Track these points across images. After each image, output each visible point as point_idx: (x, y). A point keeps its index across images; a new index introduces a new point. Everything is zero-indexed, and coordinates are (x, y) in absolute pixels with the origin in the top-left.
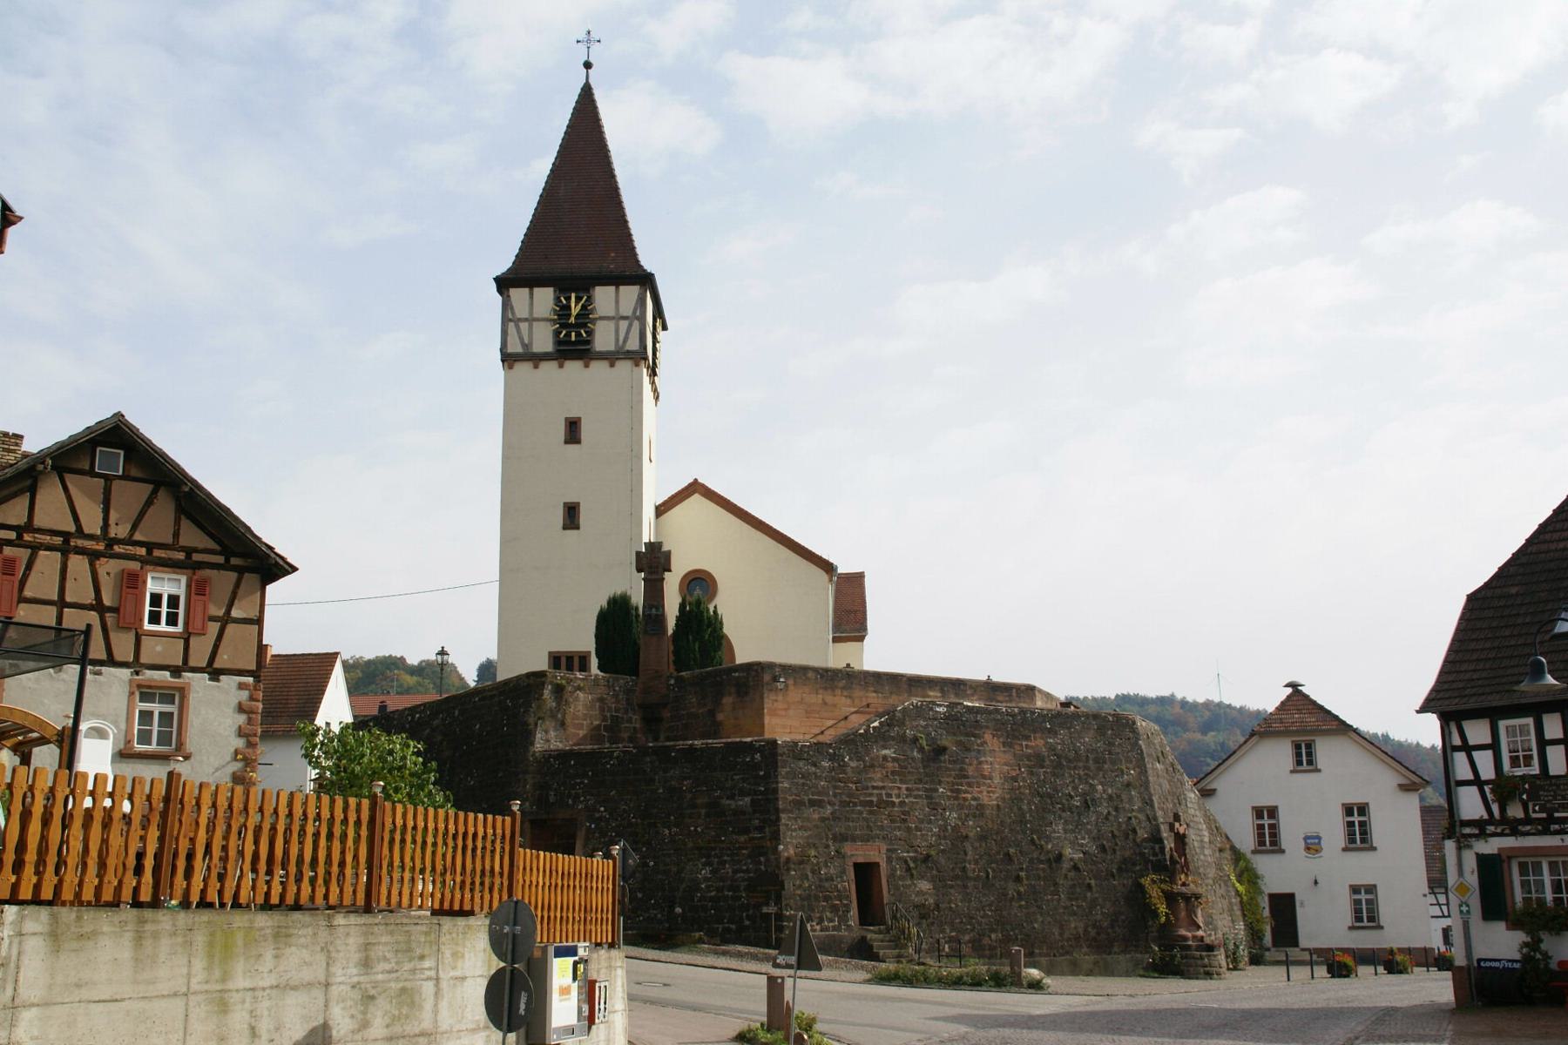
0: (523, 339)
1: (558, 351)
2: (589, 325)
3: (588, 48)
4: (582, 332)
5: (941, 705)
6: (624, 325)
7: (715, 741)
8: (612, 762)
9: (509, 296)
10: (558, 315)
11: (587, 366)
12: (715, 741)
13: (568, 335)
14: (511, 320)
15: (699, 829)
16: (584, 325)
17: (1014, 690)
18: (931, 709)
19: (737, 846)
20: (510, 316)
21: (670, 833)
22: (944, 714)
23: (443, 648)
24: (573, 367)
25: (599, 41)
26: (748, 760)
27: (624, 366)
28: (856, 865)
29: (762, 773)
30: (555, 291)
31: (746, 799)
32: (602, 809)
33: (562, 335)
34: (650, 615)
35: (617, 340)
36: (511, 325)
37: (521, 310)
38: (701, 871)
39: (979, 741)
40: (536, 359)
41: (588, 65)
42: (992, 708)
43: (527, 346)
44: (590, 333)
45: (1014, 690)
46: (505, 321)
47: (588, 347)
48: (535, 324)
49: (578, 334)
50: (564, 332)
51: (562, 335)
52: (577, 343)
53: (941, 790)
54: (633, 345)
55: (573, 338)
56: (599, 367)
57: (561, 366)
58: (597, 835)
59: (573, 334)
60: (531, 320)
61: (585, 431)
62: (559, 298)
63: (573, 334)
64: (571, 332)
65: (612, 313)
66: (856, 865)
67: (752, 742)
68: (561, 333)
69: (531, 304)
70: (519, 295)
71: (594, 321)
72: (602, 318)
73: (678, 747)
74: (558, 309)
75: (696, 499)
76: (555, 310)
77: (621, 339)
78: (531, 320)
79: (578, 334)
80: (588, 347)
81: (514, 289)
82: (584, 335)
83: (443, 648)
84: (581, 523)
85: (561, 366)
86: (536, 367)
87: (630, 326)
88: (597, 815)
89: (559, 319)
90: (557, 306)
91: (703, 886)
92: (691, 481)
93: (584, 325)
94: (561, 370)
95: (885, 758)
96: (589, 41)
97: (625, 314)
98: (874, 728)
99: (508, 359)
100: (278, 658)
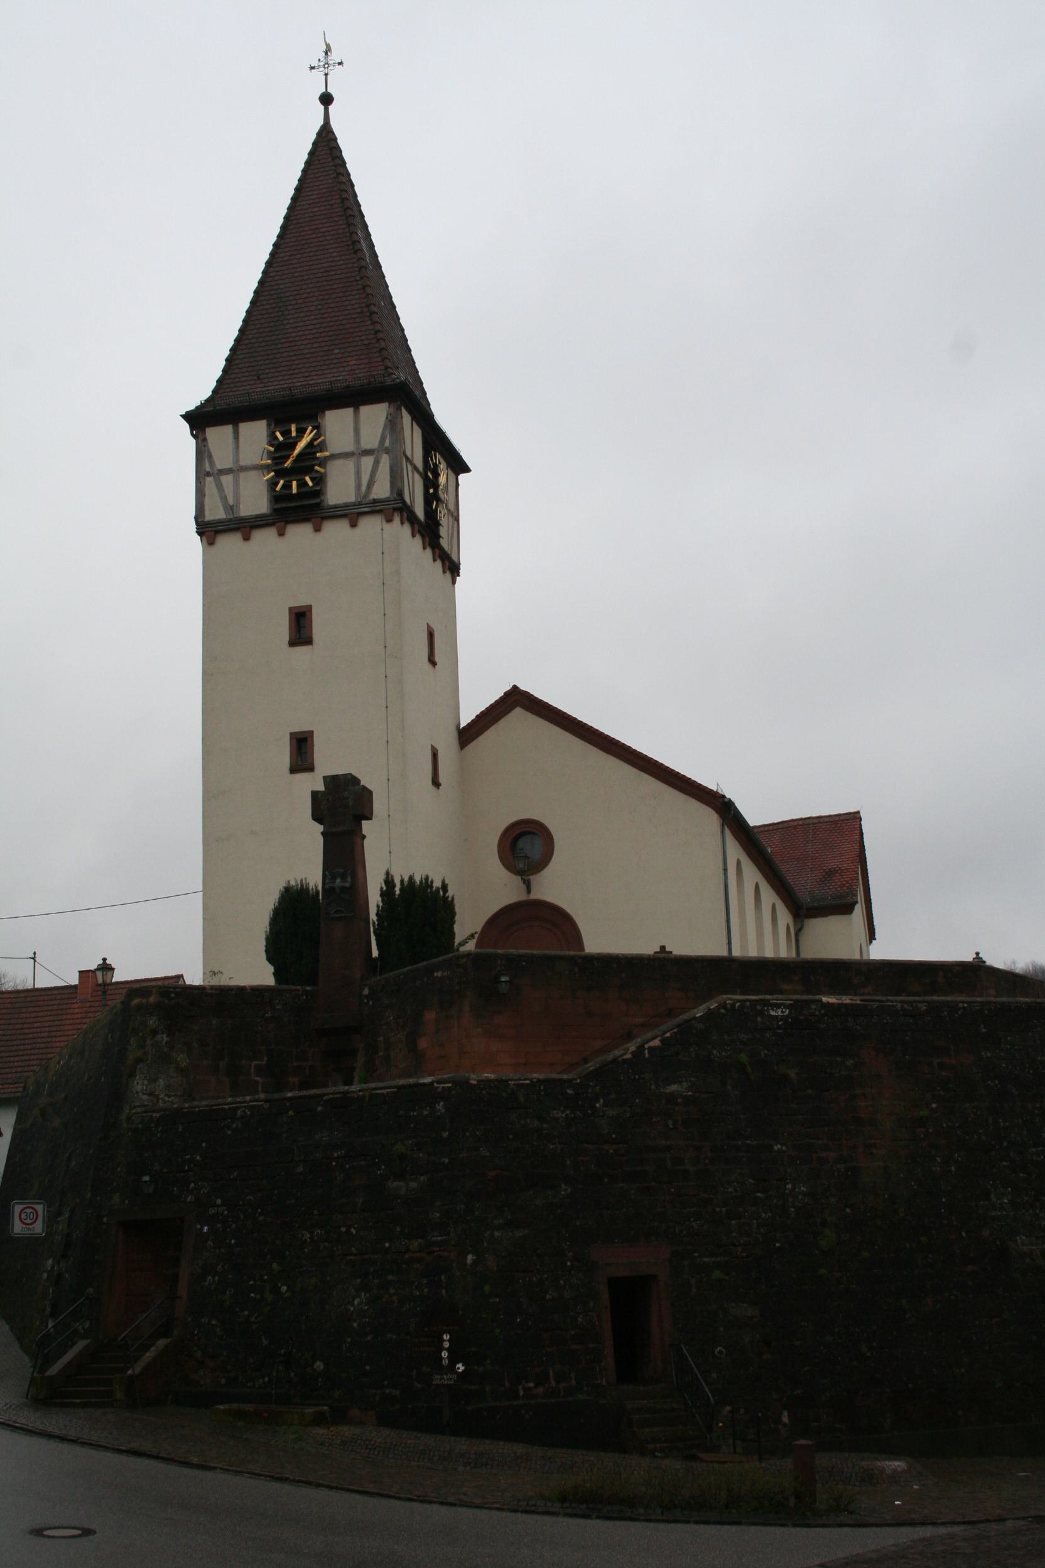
0: (226, 498)
1: (275, 510)
2: (317, 468)
3: (326, 75)
4: (307, 479)
5: (778, 1006)
6: (367, 462)
7: (381, 1085)
8: (234, 1126)
9: (205, 440)
10: (273, 459)
11: (317, 529)
12: (381, 1085)
13: (287, 486)
14: (208, 474)
15: (353, 1231)
16: (309, 470)
17: (941, 974)
18: (761, 1013)
19: (407, 1256)
20: (208, 468)
21: (311, 1238)
22: (784, 1018)
23: (977, 954)
24: (300, 533)
25: (340, 64)
26: (425, 1113)
27: (371, 525)
28: (613, 1283)
29: (445, 1135)
30: (269, 425)
31: (422, 1178)
32: (219, 1201)
33: (278, 488)
34: (333, 889)
35: (358, 486)
36: (209, 479)
37: (222, 457)
38: (354, 1299)
39: (850, 1062)
40: (245, 527)
41: (326, 99)
42: (875, 1005)
43: (232, 507)
44: (320, 480)
45: (941, 974)
46: (201, 475)
47: (318, 501)
48: (242, 475)
49: (302, 484)
50: (282, 482)
51: (278, 488)
52: (299, 496)
53: (777, 1147)
54: (382, 490)
55: (295, 491)
56: (336, 529)
57: (281, 534)
58: (210, 1243)
59: (294, 484)
60: (236, 470)
61: (319, 626)
62: (274, 433)
63: (294, 484)
64: (291, 482)
65: (350, 447)
66: (613, 1283)
67: (432, 1084)
68: (276, 484)
69: (237, 447)
70: (219, 436)
71: (323, 463)
72: (333, 457)
73: (326, 1098)
74: (272, 449)
75: (518, 713)
76: (269, 452)
77: (364, 488)
78: (236, 470)
79: (302, 484)
80: (318, 501)
81: (211, 428)
82: (310, 484)
83: (977, 954)
84: (316, 762)
85: (281, 534)
86: (247, 538)
87: (377, 462)
88: (212, 1211)
89: (276, 464)
90: (272, 446)
91: (355, 1325)
92: (508, 688)
93: (309, 470)
94: (281, 539)
95: (671, 1098)
96: (327, 64)
97: (368, 446)
98: (651, 1049)
99: (208, 530)
100: (65, 991)
